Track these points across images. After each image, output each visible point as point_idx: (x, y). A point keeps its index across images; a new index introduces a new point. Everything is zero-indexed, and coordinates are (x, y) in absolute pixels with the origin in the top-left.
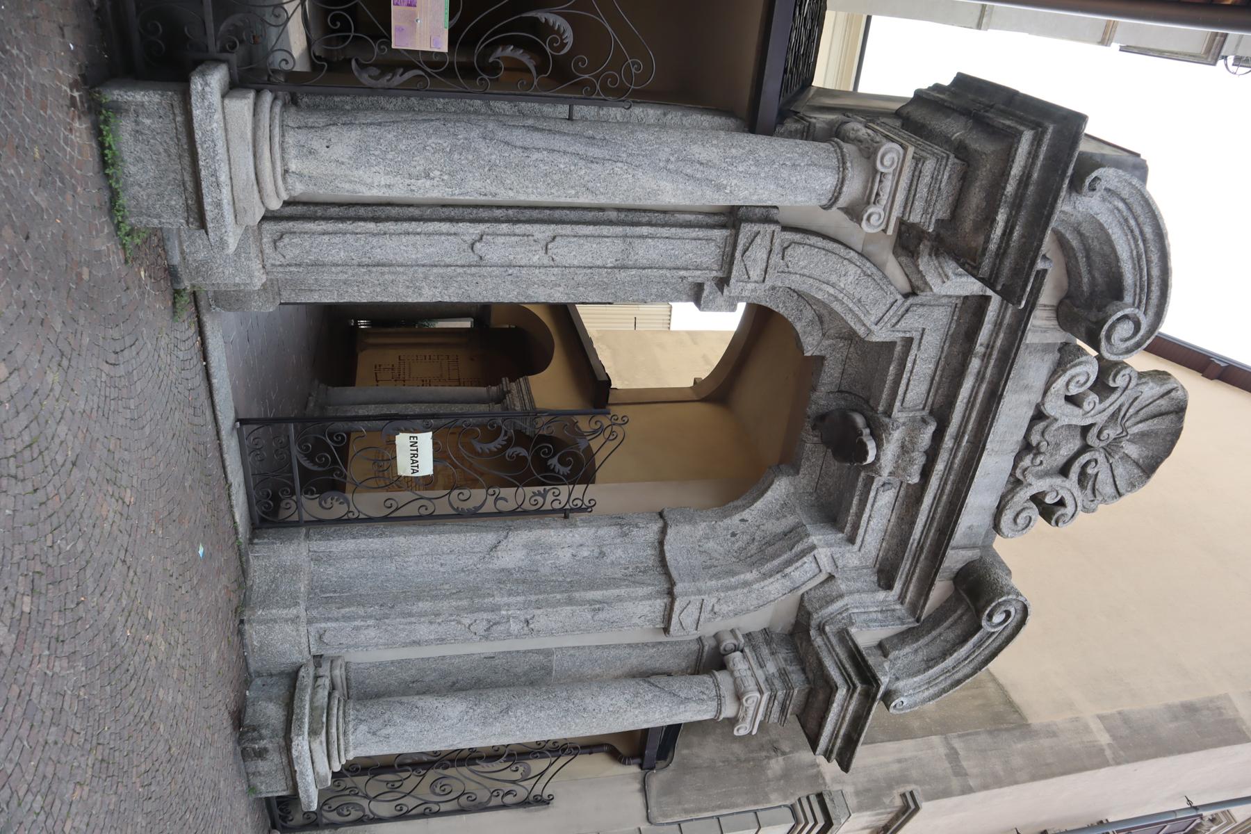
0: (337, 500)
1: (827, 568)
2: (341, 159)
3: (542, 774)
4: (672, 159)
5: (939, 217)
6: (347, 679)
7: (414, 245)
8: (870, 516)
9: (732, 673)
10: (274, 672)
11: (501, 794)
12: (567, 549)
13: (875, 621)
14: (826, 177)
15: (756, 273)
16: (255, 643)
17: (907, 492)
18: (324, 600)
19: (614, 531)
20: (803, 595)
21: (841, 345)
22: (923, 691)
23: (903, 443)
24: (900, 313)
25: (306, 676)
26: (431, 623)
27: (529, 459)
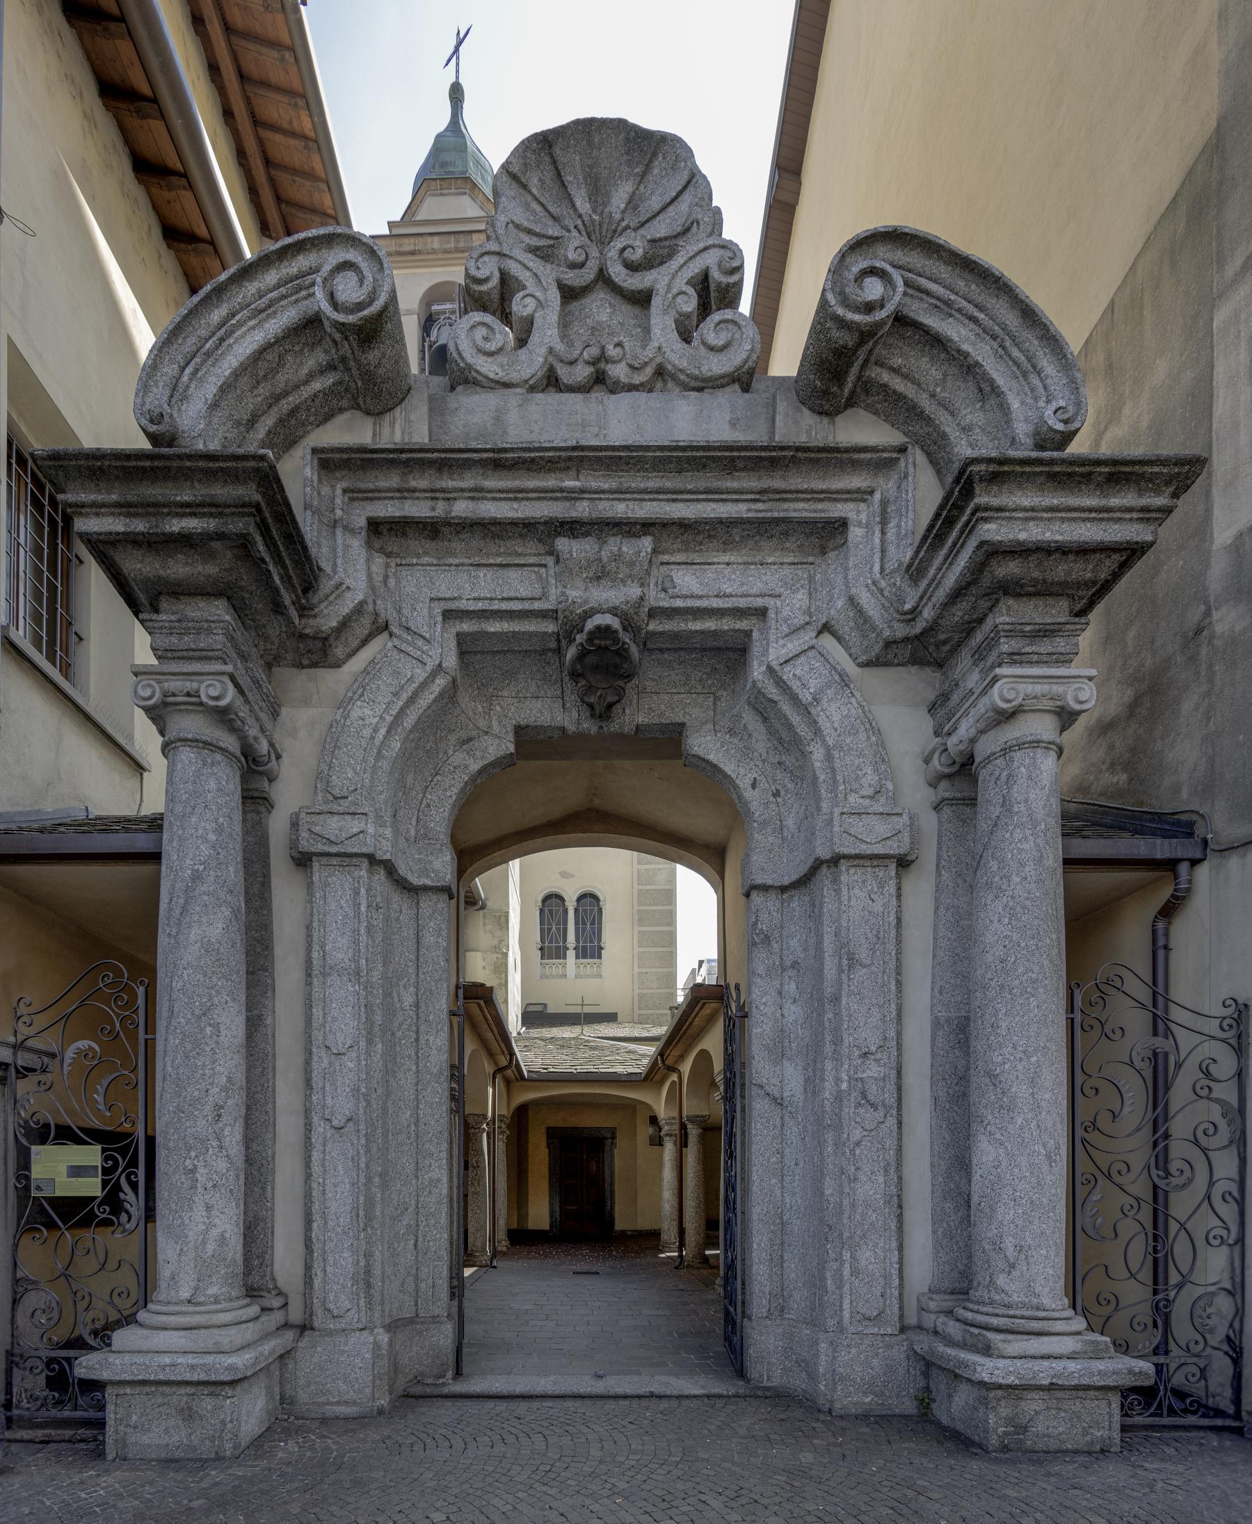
1: (807, 638)
8: (717, 596)
9: (973, 741)
14: (182, 761)
15: (355, 825)
16: (867, 1400)
17: (679, 550)
20: (861, 665)
21: (498, 708)
25: (923, 1343)
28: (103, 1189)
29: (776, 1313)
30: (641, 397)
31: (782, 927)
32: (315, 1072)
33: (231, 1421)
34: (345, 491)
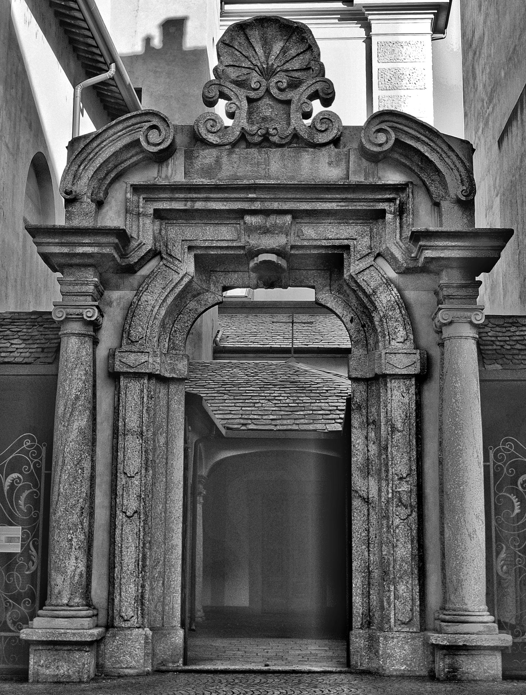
2: (63, 580)
8: (325, 239)
15: (143, 358)
16: (403, 668)
23: (262, 234)
28: (21, 549)
29: (366, 626)
30: (286, 150)
31: (367, 400)
32: (119, 487)
33: (87, 664)
34: (144, 198)
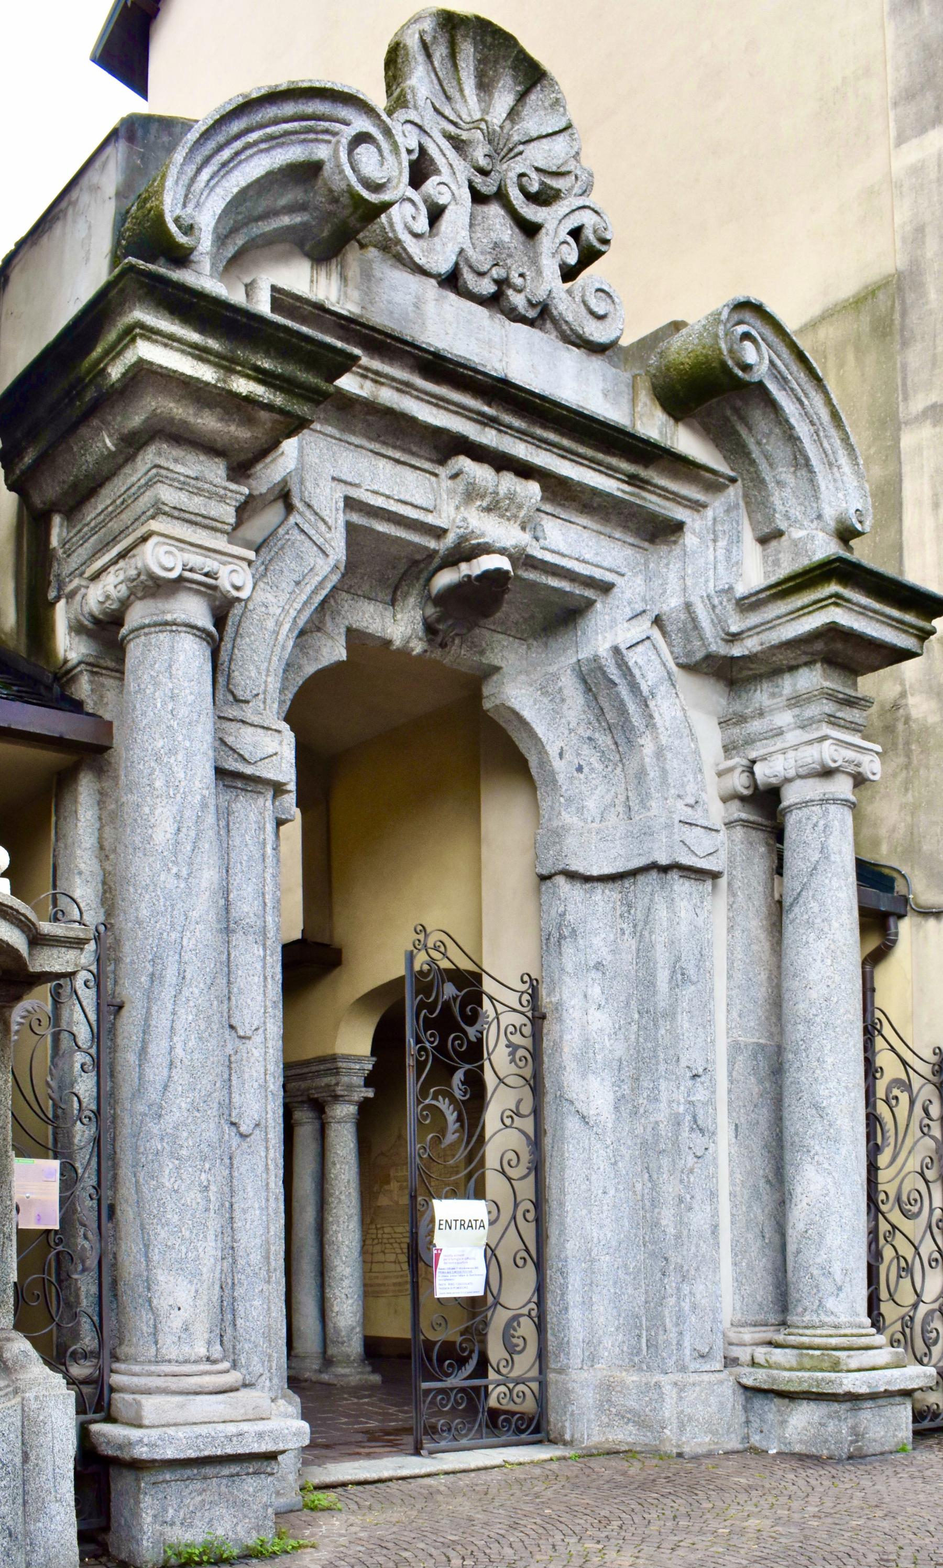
0: (515, 1330)
2: (193, 1294)
3: (904, 1063)
4: (175, 870)
5: (224, 475)
6: (755, 1325)
7: (245, 1211)
8: (577, 559)
9: (788, 780)
10: (743, 1419)
11: (926, 1121)
12: (590, 1017)
13: (728, 551)
18: (652, 1350)
19: (568, 949)
20: (678, 665)
22: (843, 475)
24: (312, 518)
26: (690, 1209)
27: (468, 1067)
